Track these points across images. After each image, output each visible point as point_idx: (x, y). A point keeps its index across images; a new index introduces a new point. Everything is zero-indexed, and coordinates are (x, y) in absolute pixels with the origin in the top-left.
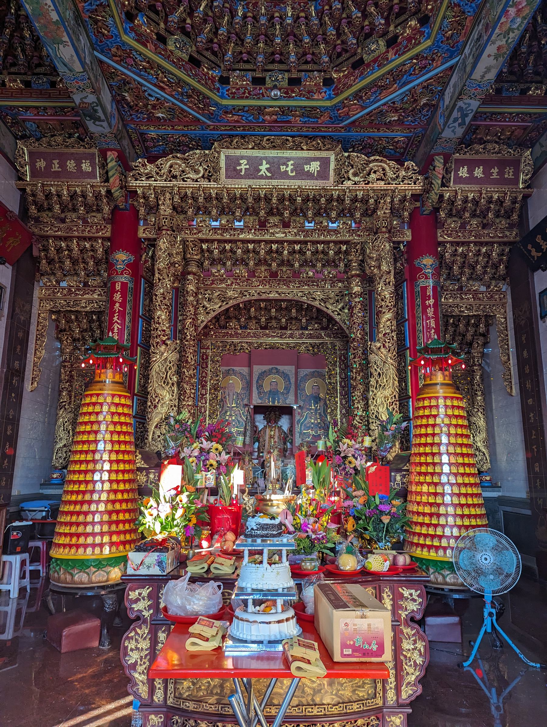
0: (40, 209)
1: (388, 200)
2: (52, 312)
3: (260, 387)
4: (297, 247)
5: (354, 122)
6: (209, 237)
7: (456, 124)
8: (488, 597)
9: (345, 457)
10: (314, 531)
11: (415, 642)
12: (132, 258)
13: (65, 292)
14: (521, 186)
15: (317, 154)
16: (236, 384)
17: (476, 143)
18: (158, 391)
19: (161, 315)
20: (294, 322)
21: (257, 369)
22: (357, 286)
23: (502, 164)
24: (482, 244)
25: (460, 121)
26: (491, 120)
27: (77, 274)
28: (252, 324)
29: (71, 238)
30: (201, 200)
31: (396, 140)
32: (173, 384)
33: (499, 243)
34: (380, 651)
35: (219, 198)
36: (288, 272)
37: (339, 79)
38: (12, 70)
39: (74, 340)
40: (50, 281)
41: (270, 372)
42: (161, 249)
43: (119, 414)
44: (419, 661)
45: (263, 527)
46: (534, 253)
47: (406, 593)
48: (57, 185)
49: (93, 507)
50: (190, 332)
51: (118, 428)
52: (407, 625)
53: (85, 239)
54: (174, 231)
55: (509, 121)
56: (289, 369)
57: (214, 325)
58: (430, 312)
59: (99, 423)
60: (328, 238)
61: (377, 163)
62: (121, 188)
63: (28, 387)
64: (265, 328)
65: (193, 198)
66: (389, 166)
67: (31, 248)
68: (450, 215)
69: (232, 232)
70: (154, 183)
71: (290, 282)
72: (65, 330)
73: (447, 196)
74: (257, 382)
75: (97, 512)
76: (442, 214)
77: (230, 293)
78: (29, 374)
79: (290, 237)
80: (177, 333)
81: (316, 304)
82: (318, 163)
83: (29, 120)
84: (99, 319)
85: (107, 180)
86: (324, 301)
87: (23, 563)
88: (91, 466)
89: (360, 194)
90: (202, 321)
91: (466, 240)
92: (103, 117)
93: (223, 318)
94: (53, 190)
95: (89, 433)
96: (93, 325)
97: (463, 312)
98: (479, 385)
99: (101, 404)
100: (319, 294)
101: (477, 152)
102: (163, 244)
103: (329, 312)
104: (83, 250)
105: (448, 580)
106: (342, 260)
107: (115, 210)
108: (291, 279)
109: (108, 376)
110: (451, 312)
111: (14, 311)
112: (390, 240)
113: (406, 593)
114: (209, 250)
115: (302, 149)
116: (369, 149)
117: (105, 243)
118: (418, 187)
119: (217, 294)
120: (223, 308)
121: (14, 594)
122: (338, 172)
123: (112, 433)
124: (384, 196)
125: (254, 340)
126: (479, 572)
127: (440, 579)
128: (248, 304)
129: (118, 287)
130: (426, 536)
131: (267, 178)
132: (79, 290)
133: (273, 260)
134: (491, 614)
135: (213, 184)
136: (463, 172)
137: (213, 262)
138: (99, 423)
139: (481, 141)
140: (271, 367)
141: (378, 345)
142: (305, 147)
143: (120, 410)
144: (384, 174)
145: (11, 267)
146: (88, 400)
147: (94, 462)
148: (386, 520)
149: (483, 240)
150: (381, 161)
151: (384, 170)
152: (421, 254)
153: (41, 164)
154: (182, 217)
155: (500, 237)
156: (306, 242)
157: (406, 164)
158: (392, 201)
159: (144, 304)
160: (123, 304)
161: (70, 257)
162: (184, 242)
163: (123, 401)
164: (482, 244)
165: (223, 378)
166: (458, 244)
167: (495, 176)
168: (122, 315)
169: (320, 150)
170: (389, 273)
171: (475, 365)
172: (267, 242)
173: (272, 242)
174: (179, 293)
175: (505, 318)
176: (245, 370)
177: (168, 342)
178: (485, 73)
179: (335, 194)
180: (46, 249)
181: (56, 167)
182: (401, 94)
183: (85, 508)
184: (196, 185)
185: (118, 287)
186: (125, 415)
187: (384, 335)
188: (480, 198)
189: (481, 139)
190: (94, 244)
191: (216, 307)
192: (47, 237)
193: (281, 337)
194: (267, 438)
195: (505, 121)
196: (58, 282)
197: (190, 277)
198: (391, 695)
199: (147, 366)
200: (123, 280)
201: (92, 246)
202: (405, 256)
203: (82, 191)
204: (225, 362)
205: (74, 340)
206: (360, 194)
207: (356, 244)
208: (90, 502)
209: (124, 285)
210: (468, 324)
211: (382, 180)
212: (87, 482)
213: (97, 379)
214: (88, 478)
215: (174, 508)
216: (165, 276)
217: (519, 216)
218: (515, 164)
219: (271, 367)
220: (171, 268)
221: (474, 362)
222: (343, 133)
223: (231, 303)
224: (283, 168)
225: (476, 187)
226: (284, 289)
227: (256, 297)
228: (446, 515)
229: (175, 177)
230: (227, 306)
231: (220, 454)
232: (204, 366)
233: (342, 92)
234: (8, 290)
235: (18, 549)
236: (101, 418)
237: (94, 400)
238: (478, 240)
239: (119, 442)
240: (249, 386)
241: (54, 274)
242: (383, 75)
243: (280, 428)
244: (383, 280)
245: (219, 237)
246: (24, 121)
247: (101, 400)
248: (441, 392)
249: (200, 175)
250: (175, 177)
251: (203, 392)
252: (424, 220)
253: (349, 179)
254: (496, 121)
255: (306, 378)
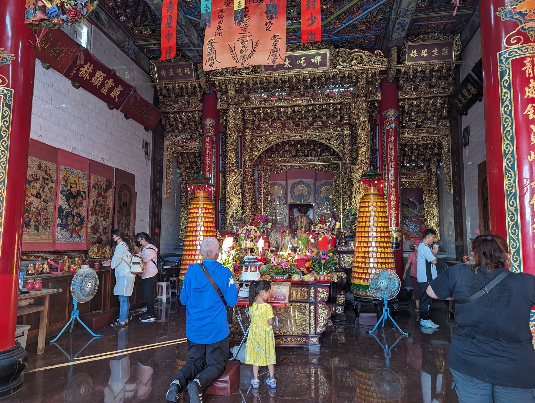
0: (164, 97)
1: (365, 76)
2: (173, 153)
3: (292, 193)
4: (310, 108)
5: (339, 31)
6: (257, 106)
7: (400, 31)
8: (386, 303)
9: (318, 234)
10: (285, 265)
11: (324, 310)
12: (215, 122)
13: (180, 142)
14: (454, 59)
15: (320, 51)
16: (279, 191)
17: (422, 34)
18: (232, 198)
19: (231, 155)
20: (313, 152)
21: (291, 182)
22: (347, 130)
23: (440, 46)
24: (430, 98)
25: (401, 29)
26: (428, 21)
27: (186, 132)
28: (288, 155)
29: (182, 112)
30: (251, 85)
31: (368, 38)
32: (239, 194)
33: (442, 97)
34: (284, 300)
35: (261, 83)
36: (306, 123)
37: (327, 9)
38: (145, 24)
39: (187, 168)
40: (172, 136)
41: (298, 183)
42: (230, 116)
43: (207, 213)
44: (325, 318)
45: (249, 259)
46: (459, 105)
47: (321, 290)
48: (172, 83)
49: (197, 257)
50: (248, 163)
51: (207, 220)
52: (321, 303)
53: (189, 112)
54: (237, 105)
55: (440, 20)
56: (310, 181)
57: (265, 155)
58: (391, 145)
59: (197, 217)
60: (329, 102)
61: (356, 53)
62: (207, 82)
63: (164, 196)
64: (295, 156)
65: (247, 84)
66: (365, 54)
67: (161, 120)
68: (407, 80)
69: (270, 102)
70: (224, 78)
71: (307, 129)
72: (181, 163)
73: (403, 70)
74: (291, 189)
75: (198, 259)
76: (401, 81)
77: (271, 138)
78: (164, 189)
79: (305, 103)
80: (241, 164)
81: (324, 141)
82: (320, 57)
83: (155, 50)
84: (200, 156)
85: (198, 79)
86: (329, 139)
87: (168, 286)
88: (194, 238)
89: (346, 74)
90: (256, 156)
91: (418, 96)
92: (193, 49)
93: (269, 151)
94: (170, 86)
95: (193, 222)
96: (197, 159)
97: (420, 141)
98: (434, 187)
99: (198, 208)
100: (325, 136)
101: (423, 40)
102: (231, 113)
103: (332, 146)
104: (188, 118)
105: (368, 294)
106: (339, 115)
107: (204, 94)
108: (308, 127)
109: (201, 194)
110: (411, 142)
111: (154, 155)
112: (366, 101)
113: (321, 290)
114: (258, 113)
115: (310, 50)
116: (351, 45)
117: (200, 113)
118: (384, 66)
119: (264, 139)
120: (268, 147)
121: (164, 301)
122: (332, 61)
123: (204, 222)
124: (361, 74)
125: (289, 164)
126: (379, 289)
127: (364, 294)
128: (284, 143)
129: (207, 140)
130: (362, 273)
131: (289, 68)
132: (187, 140)
133: (296, 116)
134: (386, 310)
135: (258, 75)
136: (414, 54)
137: (261, 120)
138: (197, 217)
139: (425, 33)
140: (299, 180)
141: (357, 167)
142: (311, 48)
143: (207, 211)
144: (362, 60)
145: (151, 132)
146: (192, 206)
147: (196, 236)
148: (323, 262)
149: (429, 96)
150: (359, 52)
151: (361, 57)
152: (387, 108)
153: (163, 72)
154: (241, 95)
155: (441, 93)
156: (315, 105)
157: (375, 52)
158: (367, 76)
159: (222, 148)
160: (211, 149)
161: (181, 122)
162: (243, 110)
163: (208, 206)
164: (430, 98)
165: (271, 187)
166: (414, 99)
167: (435, 54)
168: (210, 157)
169: (321, 49)
170: (365, 122)
171: (433, 174)
172: (292, 106)
173: (295, 106)
174: (241, 140)
175: (449, 144)
176: (284, 183)
177: (236, 170)
178: (409, 5)
179: (331, 75)
180: (169, 119)
181: (171, 73)
182: (365, 15)
183: (193, 257)
184: (248, 76)
185: (207, 140)
186: (210, 213)
187: (362, 161)
188: (426, 69)
189: (425, 31)
190: (194, 114)
191: (264, 147)
192: (169, 113)
193: (305, 161)
194: (299, 222)
195: (437, 21)
196: (176, 136)
197: (247, 131)
198: (312, 330)
199: (225, 184)
200: (210, 135)
201: (193, 115)
202: (378, 109)
203: (186, 86)
204: (272, 178)
205: (187, 168)
206: (346, 74)
207: (346, 104)
208: (195, 255)
209: (211, 138)
210: (426, 148)
211: (361, 63)
212: (193, 246)
213: (196, 196)
214: (194, 243)
215: (228, 256)
216: (232, 132)
217: (454, 79)
218: (449, 45)
219: (299, 180)
220: (236, 127)
221: (431, 172)
222: (334, 38)
223: (272, 144)
224: (298, 62)
225: (423, 62)
226: (304, 133)
227: (287, 139)
228: (374, 263)
229: (236, 73)
230: (270, 146)
231: (256, 232)
232: (260, 181)
233: (329, 17)
234: (151, 145)
235: (165, 279)
236: (198, 215)
237: (195, 206)
238: (426, 96)
239: (207, 227)
240: (286, 193)
241: (174, 132)
242: (351, 7)
243: (308, 217)
244: (361, 127)
245: (263, 106)
246: (153, 50)
247: (198, 206)
248: (372, 198)
249: (250, 70)
250: (236, 73)
251: (260, 196)
252: (390, 84)
253: (340, 65)
254: (431, 21)
255: (321, 186)
